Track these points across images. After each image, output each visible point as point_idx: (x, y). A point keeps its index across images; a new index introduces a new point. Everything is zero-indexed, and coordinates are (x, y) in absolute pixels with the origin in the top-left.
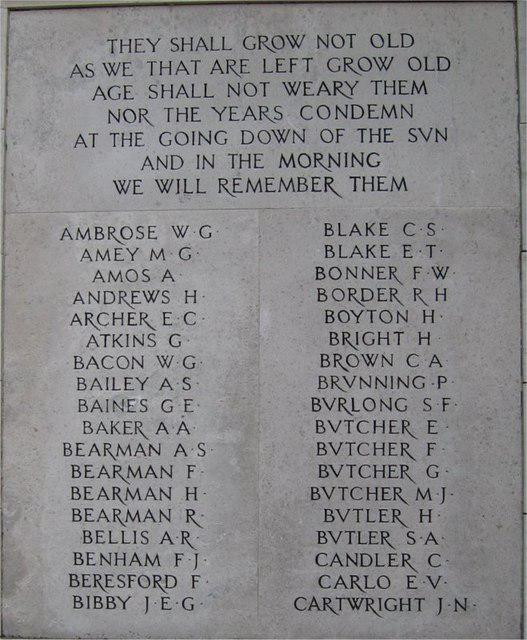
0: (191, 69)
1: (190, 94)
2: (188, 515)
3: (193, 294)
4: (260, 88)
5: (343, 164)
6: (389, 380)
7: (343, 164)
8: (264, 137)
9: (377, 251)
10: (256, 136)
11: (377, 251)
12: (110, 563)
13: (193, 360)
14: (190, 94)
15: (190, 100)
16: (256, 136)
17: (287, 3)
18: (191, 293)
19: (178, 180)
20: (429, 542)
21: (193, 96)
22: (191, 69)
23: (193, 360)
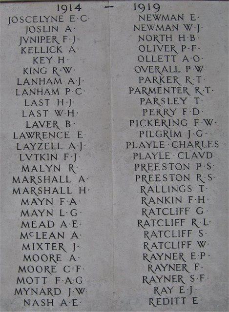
0: (158, 235)
1: (169, 71)
2: (145, 234)
3: (202, 198)
4: (35, 280)
5: (37, 41)
6: (37, 39)
7: (37, 41)
8: (36, 258)
9: (38, 60)
10: (35, 269)
11: (38, 60)
12: (34, 69)
13: (201, 133)
14: (169, 71)
15: (60, 194)
16: (35, 269)
17: (35, 1)
18: (182, 36)
19: (31, 68)
20: (34, 127)
21: (61, 182)
22: (158, 235)
23: (201, 133)
